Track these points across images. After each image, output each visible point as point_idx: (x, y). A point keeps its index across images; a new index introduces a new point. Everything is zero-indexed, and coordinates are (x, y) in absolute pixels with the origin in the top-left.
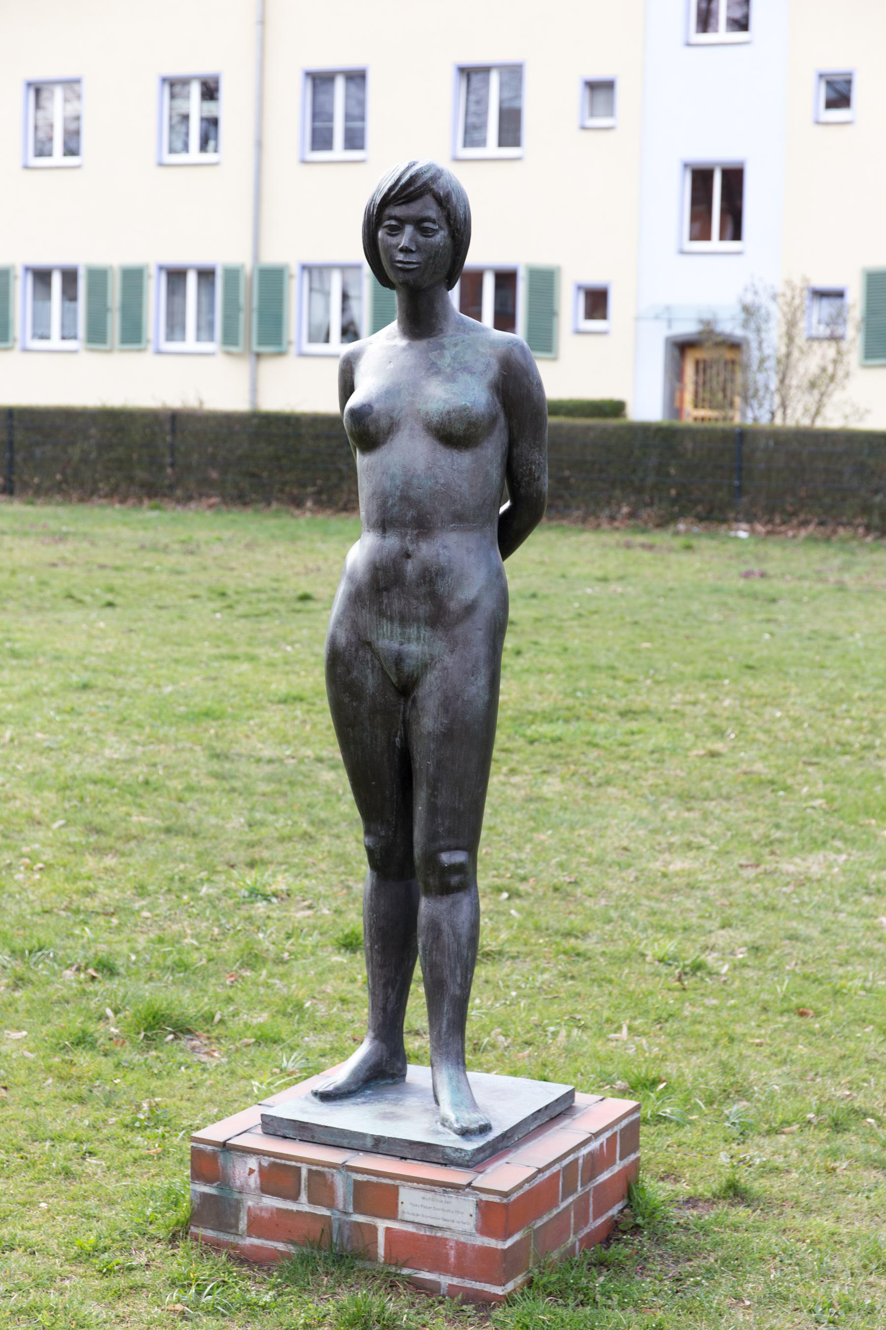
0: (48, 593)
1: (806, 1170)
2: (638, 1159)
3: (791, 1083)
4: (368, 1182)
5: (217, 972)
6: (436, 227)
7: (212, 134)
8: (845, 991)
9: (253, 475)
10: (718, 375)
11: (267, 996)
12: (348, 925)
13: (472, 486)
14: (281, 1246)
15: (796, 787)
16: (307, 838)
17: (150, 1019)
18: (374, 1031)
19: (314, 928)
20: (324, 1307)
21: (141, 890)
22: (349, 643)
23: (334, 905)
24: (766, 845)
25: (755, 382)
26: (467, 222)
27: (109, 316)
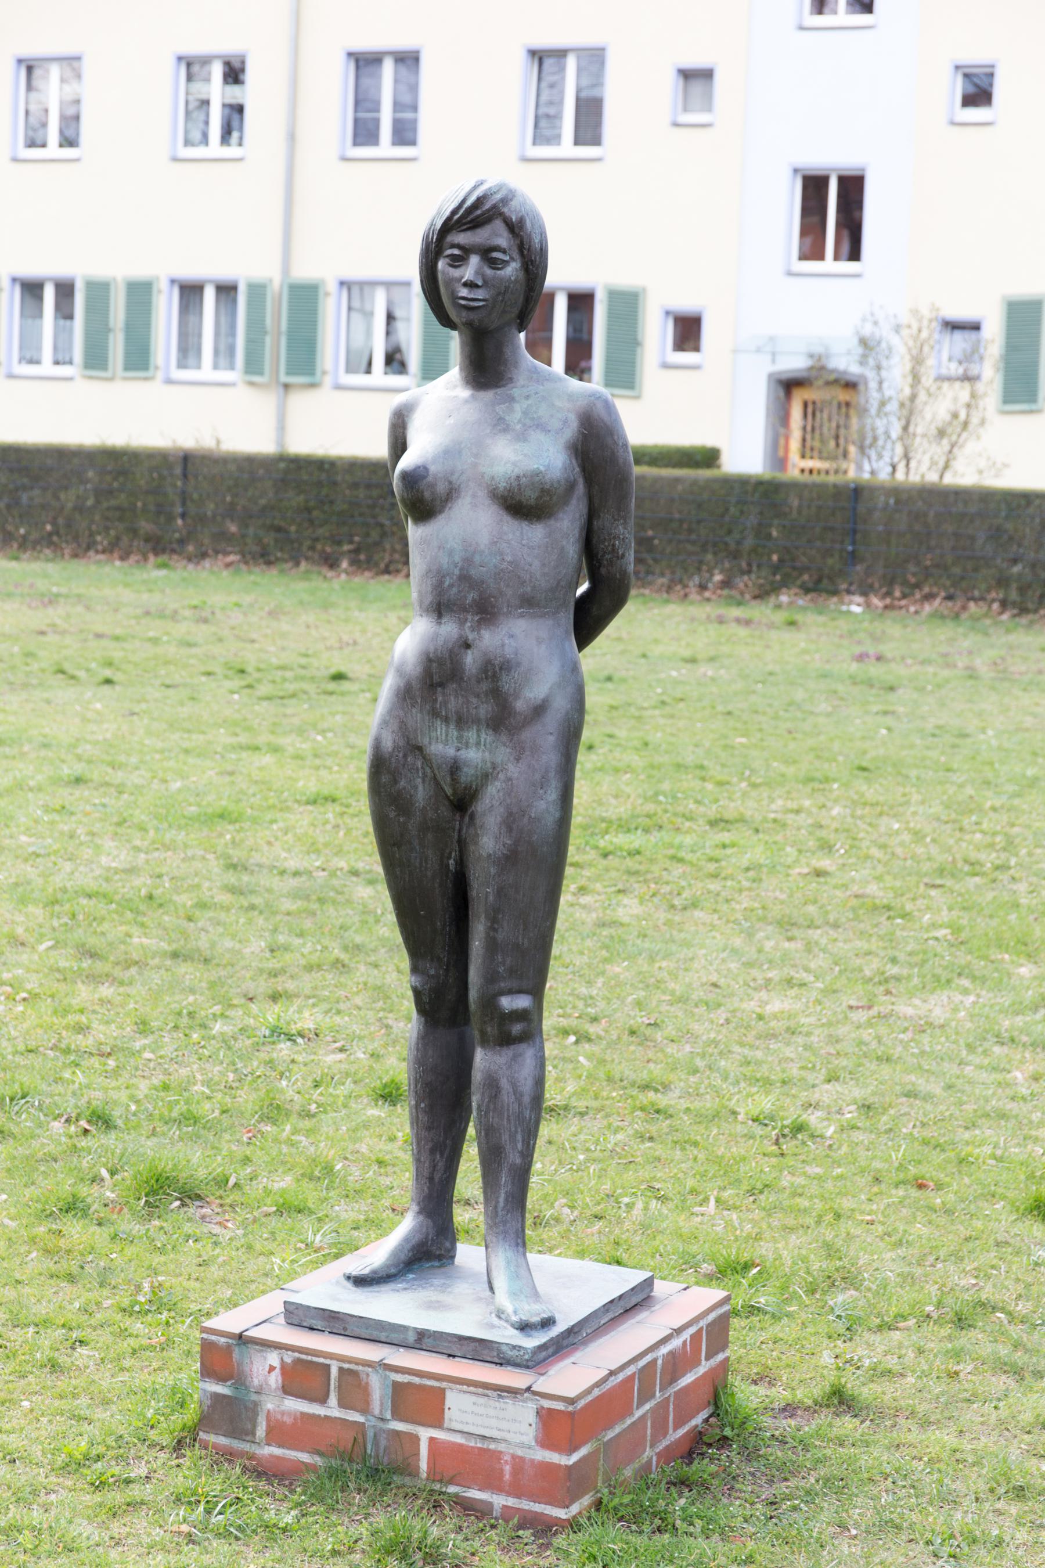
0: (35, 666)
1: (925, 1374)
2: (727, 1359)
3: (907, 1269)
4: (409, 1383)
5: (232, 1126)
6: (507, 258)
7: (235, 123)
8: (971, 1159)
9: (279, 529)
10: (830, 420)
11: (291, 1155)
12: (387, 1071)
13: (544, 565)
14: (305, 1457)
15: (916, 913)
16: (339, 966)
17: (153, 1181)
18: (419, 1204)
19: (347, 1074)
20: (356, 1530)
21: (143, 1027)
22: (396, 747)
23: (370, 1047)
24: (880, 983)
25: (873, 429)
26: (543, 253)
27: (111, 336)
